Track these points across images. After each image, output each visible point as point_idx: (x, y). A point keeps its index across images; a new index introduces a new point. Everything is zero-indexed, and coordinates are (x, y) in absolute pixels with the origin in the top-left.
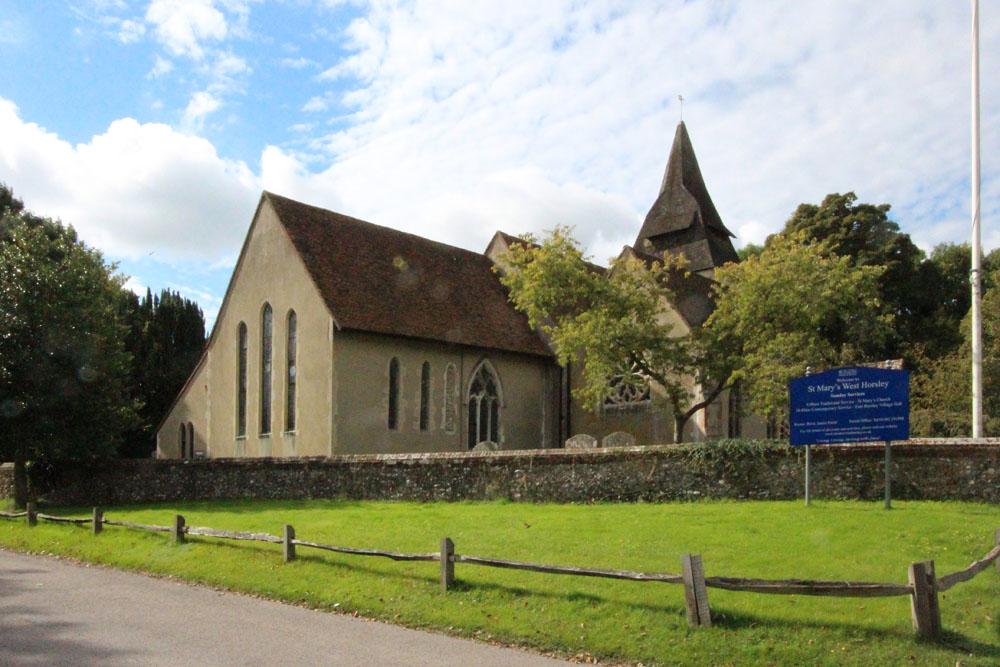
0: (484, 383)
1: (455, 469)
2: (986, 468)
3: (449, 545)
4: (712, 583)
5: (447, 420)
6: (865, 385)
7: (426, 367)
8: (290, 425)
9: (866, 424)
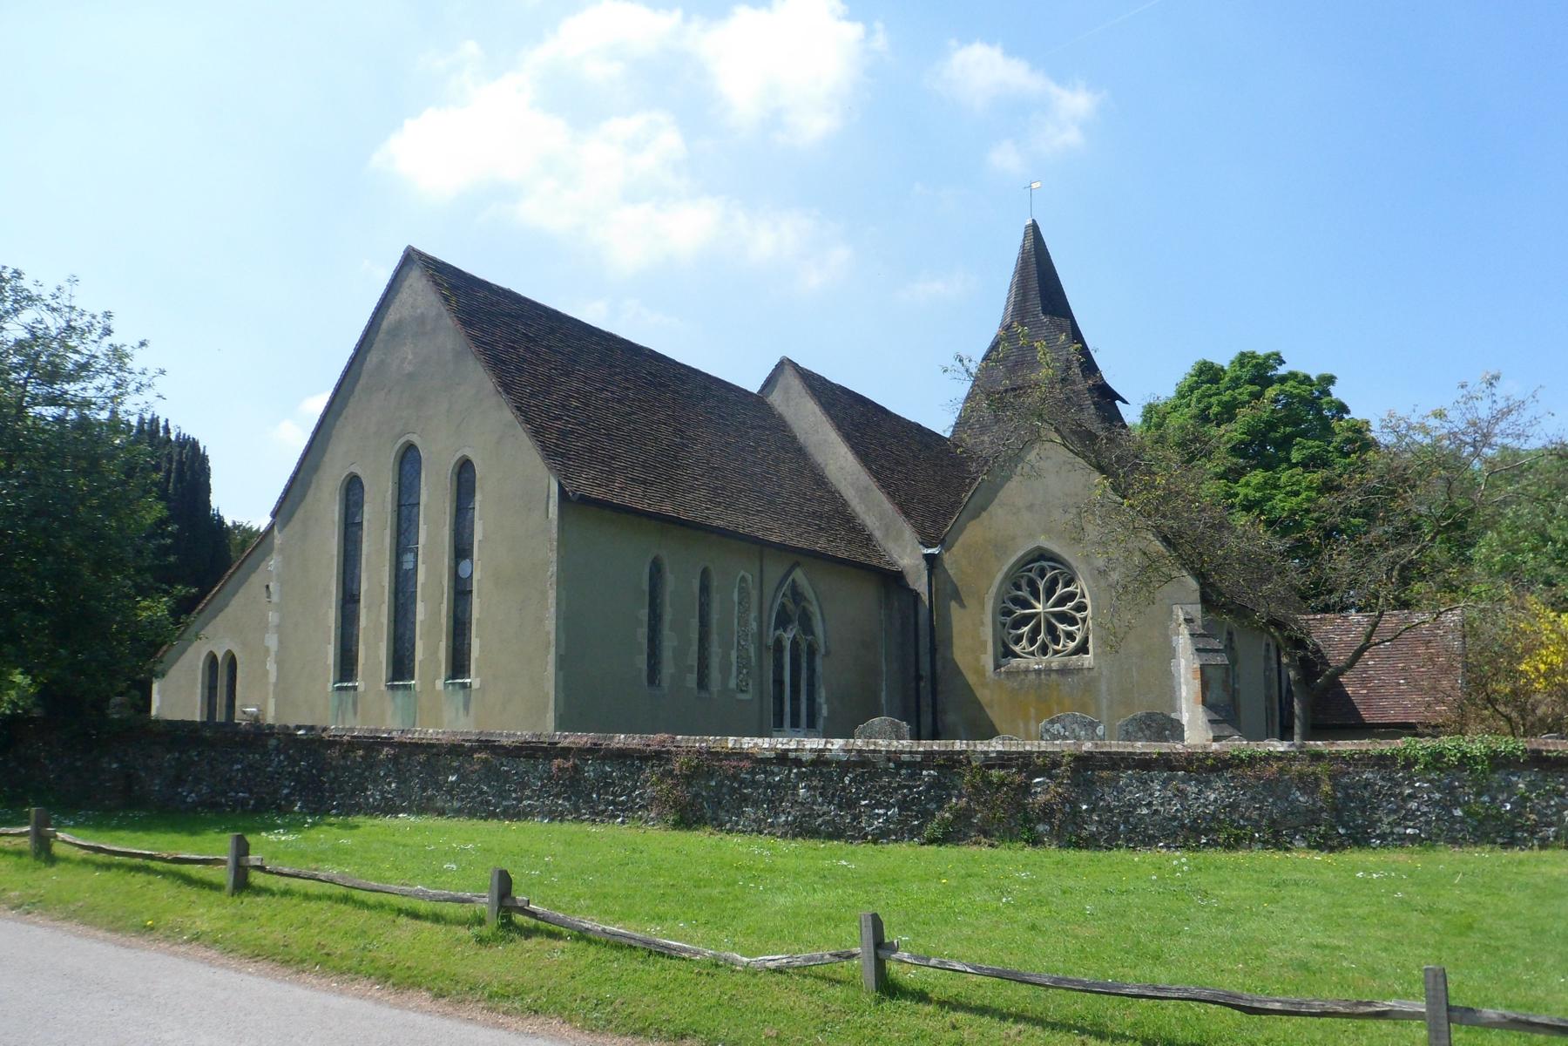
0: (793, 612)
1: (903, 771)
3: (504, 883)
5: (739, 673)
7: (705, 574)
8: (459, 665)
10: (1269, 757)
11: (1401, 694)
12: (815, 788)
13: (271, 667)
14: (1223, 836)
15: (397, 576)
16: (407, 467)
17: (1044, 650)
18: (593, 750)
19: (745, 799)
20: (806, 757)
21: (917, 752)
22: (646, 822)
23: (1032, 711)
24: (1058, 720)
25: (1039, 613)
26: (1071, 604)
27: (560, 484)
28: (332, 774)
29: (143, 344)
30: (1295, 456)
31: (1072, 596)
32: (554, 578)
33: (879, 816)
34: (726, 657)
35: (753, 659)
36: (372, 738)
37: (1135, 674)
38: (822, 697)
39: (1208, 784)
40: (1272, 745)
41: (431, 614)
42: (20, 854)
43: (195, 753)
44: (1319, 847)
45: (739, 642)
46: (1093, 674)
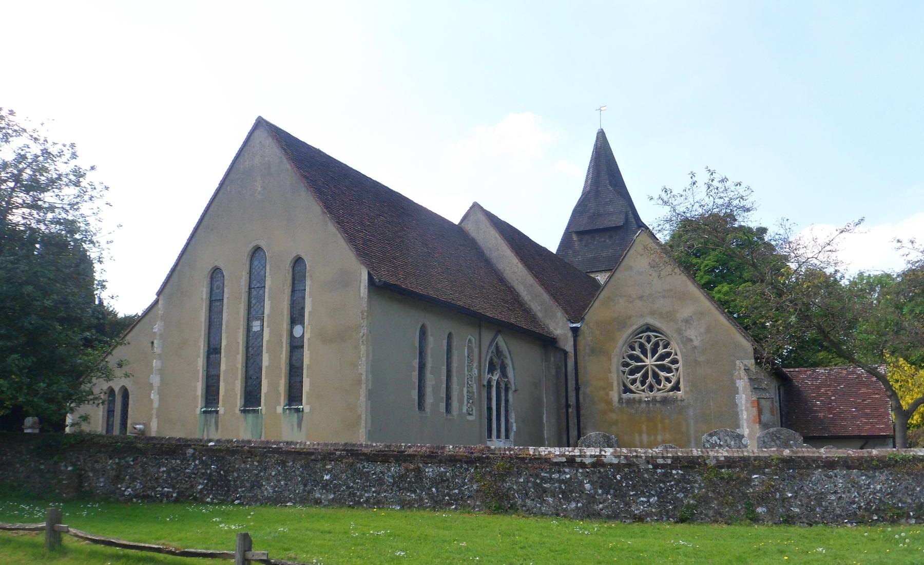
8: (294, 396)
11: (854, 417)
13: (154, 396)
15: (248, 336)
16: (256, 263)
17: (651, 388)
21: (668, 457)
22: (474, 508)
23: (644, 428)
24: (715, 434)
25: (648, 365)
26: (668, 360)
27: (369, 274)
28: (235, 474)
29: (93, 168)
31: (668, 355)
34: (461, 391)
35: (475, 394)
36: (265, 448)
37: (712, 404)
38: (512, 420)
40: (913, 451)
42: (34, 545)
43: (132, 459)
46: (683, 403)
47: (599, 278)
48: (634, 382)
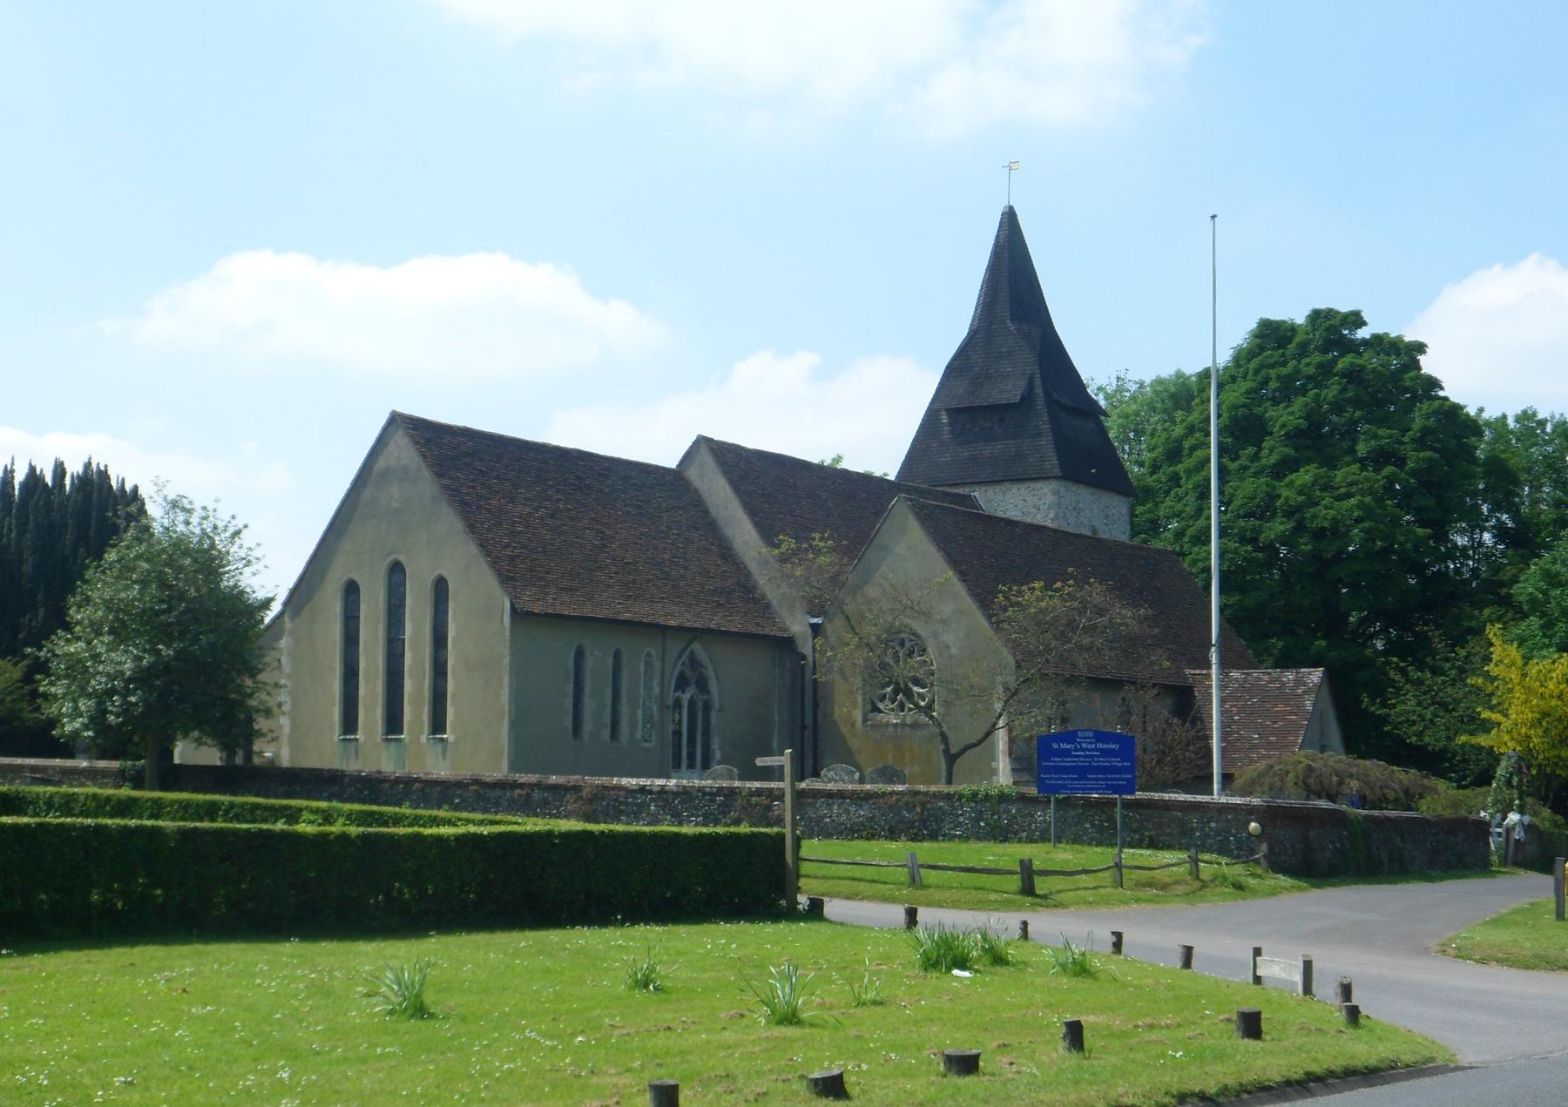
0: (692, 677)
1: (706, 798)
2: (1209, 822)
4: (922, 866)
5: (644, 726)
6: (1100, 746)
8: (438, 725)
9: (1102, 779)
10: (893, 793)
12: (659, 806)
14: (865, 833)
18: (538, 785)
19: (621, 812)
20: (655, 789)
27: (511, 602)
30: (1362, 449)
32: (507, 668)
33: (692, 821)
38: (716, 744)
39: (860, 806)
41: (416, 686)
44: (913, 840)
45: (644, 704)
47: (976, 494)
48: (883, 698)
